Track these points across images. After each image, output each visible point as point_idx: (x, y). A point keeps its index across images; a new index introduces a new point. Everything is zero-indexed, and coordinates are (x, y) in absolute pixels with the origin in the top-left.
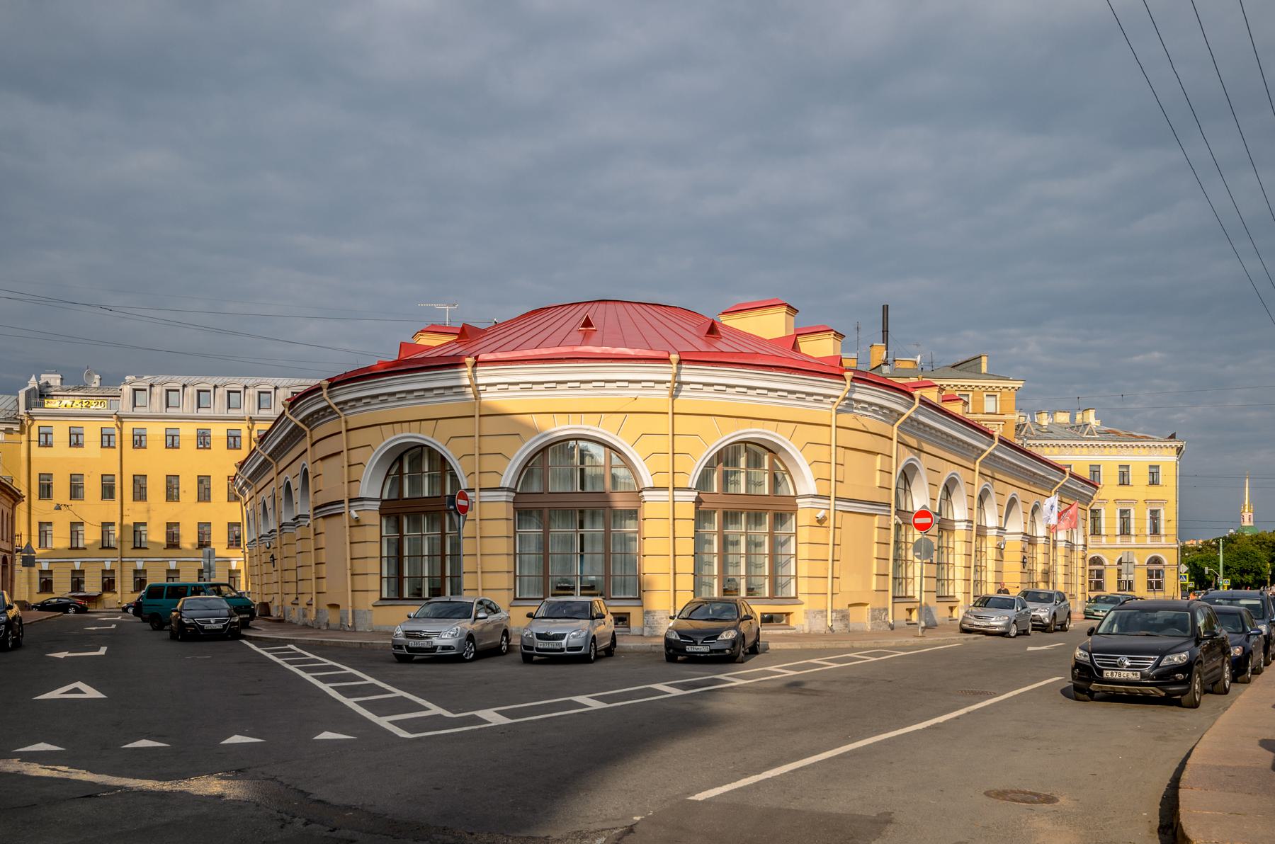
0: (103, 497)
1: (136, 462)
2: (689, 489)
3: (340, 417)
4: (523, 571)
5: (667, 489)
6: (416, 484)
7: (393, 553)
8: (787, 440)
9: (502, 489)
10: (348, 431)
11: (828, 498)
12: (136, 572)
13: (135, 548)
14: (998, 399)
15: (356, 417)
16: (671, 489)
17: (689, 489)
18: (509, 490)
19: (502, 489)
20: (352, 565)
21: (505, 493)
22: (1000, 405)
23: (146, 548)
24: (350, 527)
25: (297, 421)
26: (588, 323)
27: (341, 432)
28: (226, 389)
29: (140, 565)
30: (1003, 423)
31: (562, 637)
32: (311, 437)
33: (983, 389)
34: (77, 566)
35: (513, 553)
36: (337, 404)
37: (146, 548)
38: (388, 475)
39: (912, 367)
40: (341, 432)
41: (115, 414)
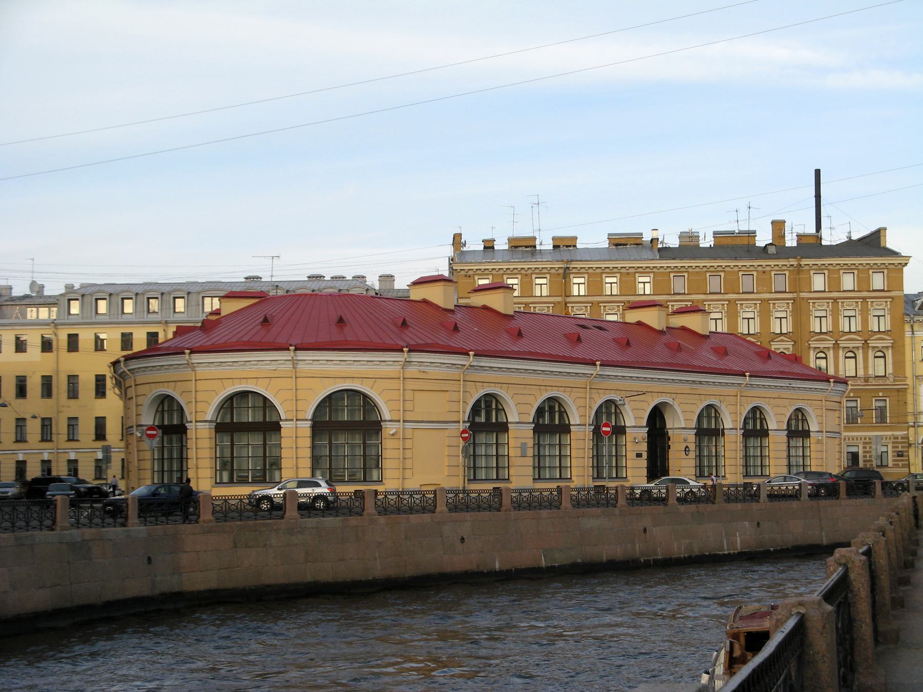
0: (43, 397)
1: (70, 363)
2: (306, 420)
3: (130, 377)
4: (476, 451)
5: (292, 420)
6: (171, 417)
7: (179, 457)
8: (369, 390)
9: (206, 421)
10: (136, 385)
11: (399, 421)
12: (70, 461)
13: (69, 440)
14: (885, 275)
15: (141, 378)
16: (295, 420)
17: (306, 420)
18: (211, 421)
19: (206, 421)
20: (138, 464)
21: (208, 424)
22: (888, 281)
23: (78, 440)
24: (138, 441)
25: (125, 369)
26: (266, 320)
27: (131, 386)
28: (146, 297)
29: (72, 456)
30: (891, 300)
31: (8, 492)
32: (125, 386)
33: (868, 267)
34: (21, 457)
35: (214, 456)
36: (129, 370)
37: (78, 440)
38: (157, 411)
39: (815, 242)
40: (131, 386)
41: (53, 323)
